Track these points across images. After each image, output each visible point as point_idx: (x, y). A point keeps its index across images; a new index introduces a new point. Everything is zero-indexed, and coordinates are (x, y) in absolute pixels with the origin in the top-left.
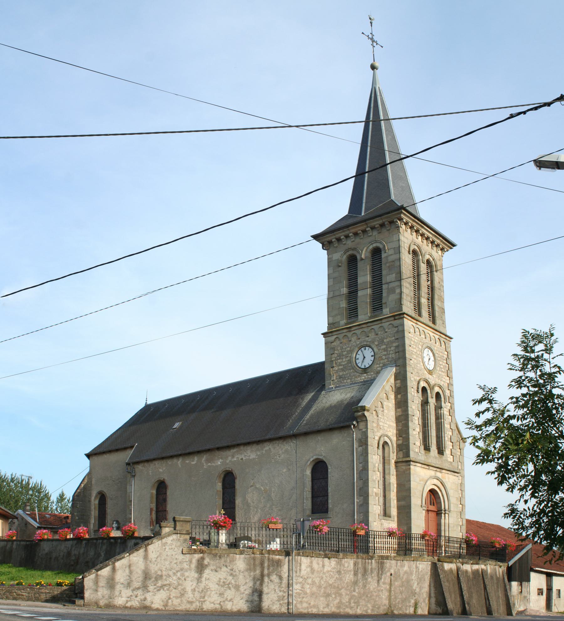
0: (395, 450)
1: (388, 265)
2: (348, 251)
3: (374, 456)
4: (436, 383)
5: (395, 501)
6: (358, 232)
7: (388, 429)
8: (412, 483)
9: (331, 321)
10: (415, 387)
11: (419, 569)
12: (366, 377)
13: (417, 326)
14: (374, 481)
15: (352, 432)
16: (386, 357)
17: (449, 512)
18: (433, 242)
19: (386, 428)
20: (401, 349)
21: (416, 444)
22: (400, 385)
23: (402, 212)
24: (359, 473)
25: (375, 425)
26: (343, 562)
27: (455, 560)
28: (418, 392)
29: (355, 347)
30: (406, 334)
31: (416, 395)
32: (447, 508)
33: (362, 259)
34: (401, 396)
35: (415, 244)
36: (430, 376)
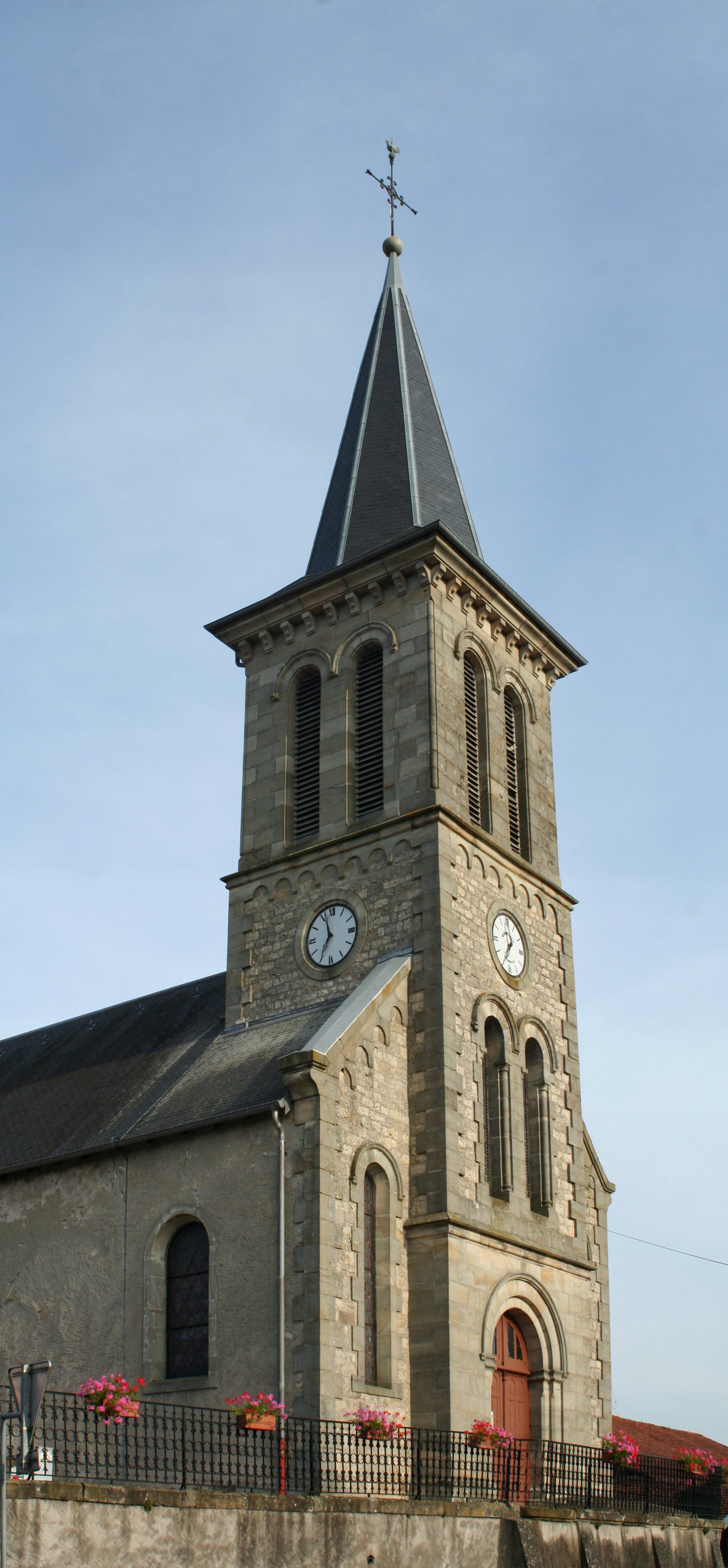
0: (406, 1193)
1: (397, 683)
2: (298, 659)
3: (337, 1203)
4: (528, 1013)
5: (405, 1342)
6: (325, 607)
7: (385, 1129)
8: (452, 1286)
9: (249, 847)
10: (467, 1015)
11: (461, 1542)
12: (334, 989)
13: (477, 852)
14: (338, 1277)
15: (276, 1132)
16: (388, 930)
17: (563, 1376)
18: (521, 645)
19: (377, 1126)
20: (427, 904)
21: (466, 1175)
22: (422, 1004)
23: (435, 543)
24: (294, 1254)
25: (342, 1112)
26: (200, 1519)
27: (572, 1514)
28: (474, 1029)
29: (307, 907)
30: (443, 865)
31: (468, 1036)
32: (557, 1364)
33: (332, 676)
34: (426, 1036)
35: (472, 638)
36: (511, 992)
